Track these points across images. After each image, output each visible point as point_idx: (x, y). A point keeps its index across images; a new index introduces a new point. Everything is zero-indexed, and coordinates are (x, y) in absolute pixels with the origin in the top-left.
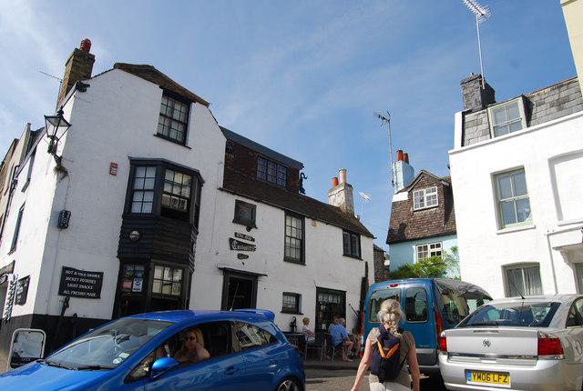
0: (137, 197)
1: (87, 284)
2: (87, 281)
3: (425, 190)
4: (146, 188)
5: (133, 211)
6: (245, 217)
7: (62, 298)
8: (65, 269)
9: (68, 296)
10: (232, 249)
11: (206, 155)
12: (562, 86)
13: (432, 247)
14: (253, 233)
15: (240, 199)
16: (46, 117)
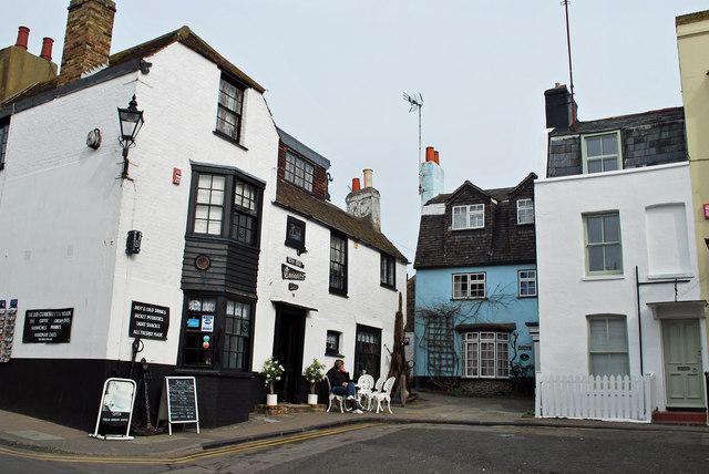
0: (201, 214)
1: (151, 322)
2: (154, 318)
3: (468, 207)
4: (672, 286)
5: (196, 231)
6: (296, 240)
7: (133, 340)
8: (135, 304)
9: (138, 338)
10: (284, 278)
11: (260, 162)
12: (664, 125)
13: (473, 278)
14: (303, 258)
15: (291, 215)
16: (120, 110)
